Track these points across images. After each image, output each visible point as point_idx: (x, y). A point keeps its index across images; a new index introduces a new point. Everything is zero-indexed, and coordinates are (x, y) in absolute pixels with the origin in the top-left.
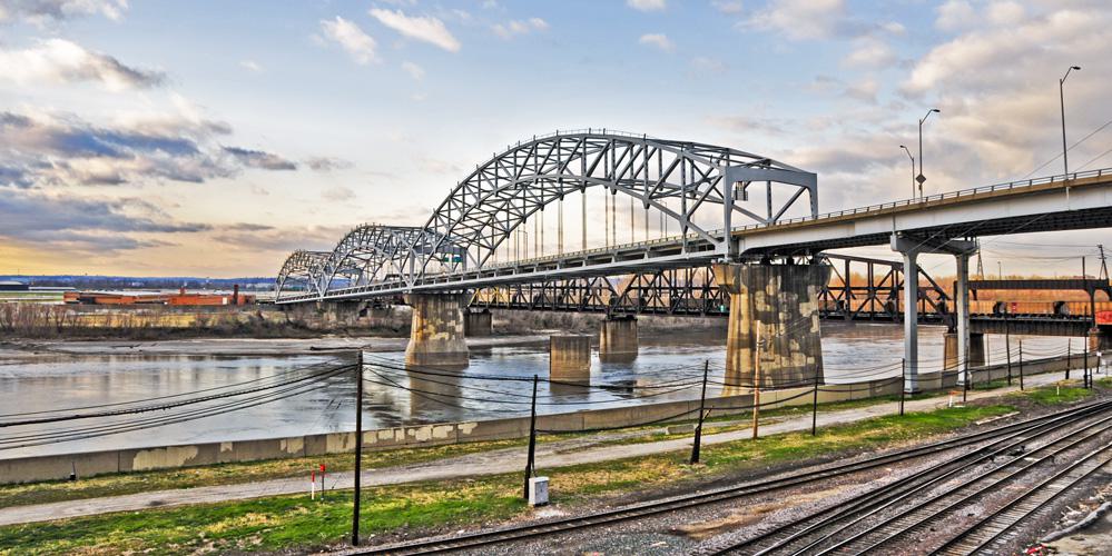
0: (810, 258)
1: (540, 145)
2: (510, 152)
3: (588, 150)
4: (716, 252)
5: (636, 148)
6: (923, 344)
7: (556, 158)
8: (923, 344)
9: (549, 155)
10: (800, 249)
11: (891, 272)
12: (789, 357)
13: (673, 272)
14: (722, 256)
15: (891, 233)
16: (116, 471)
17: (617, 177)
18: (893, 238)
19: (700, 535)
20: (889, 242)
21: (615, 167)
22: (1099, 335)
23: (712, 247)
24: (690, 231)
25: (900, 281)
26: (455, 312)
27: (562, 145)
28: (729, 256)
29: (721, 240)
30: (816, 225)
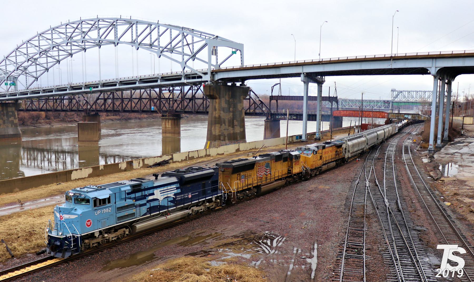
0: (241, 83)
1: (83, 23)
2: (62, 25)
3: (118, 23)
4: (203, 79)
5: (153, 27)
6: (182, 130)
7: (97, 25)
8: (182, 130)
9: (94, 24)
10: (237, 79)
11: (203, 103)
12: (233, 127)
13: (183, 87)
14: (207, 81)
15: (301, 73)
16: (88, 34)
17: (138, 42)
18: (302, 75)
19: (56, 193)
20: (300, 76)
21: (138, 36)
22: (334, 119)
23: (201, 77)
24: (186, 69)
25: (208, 105)
26: (13, 112)
27: (100, 23)
28: (211, 81)
29: (205, 74)
30: (242, 69)
